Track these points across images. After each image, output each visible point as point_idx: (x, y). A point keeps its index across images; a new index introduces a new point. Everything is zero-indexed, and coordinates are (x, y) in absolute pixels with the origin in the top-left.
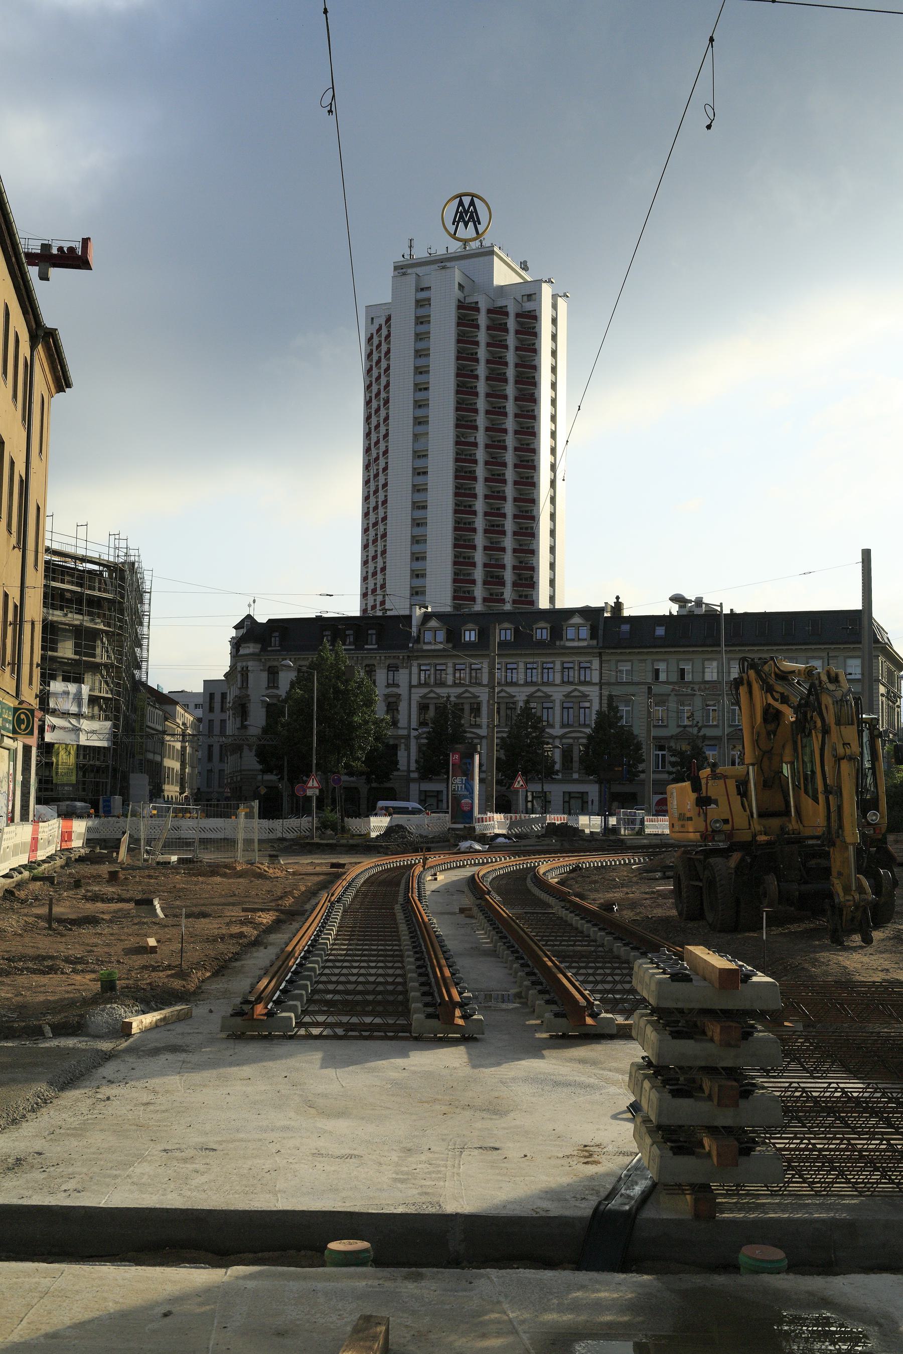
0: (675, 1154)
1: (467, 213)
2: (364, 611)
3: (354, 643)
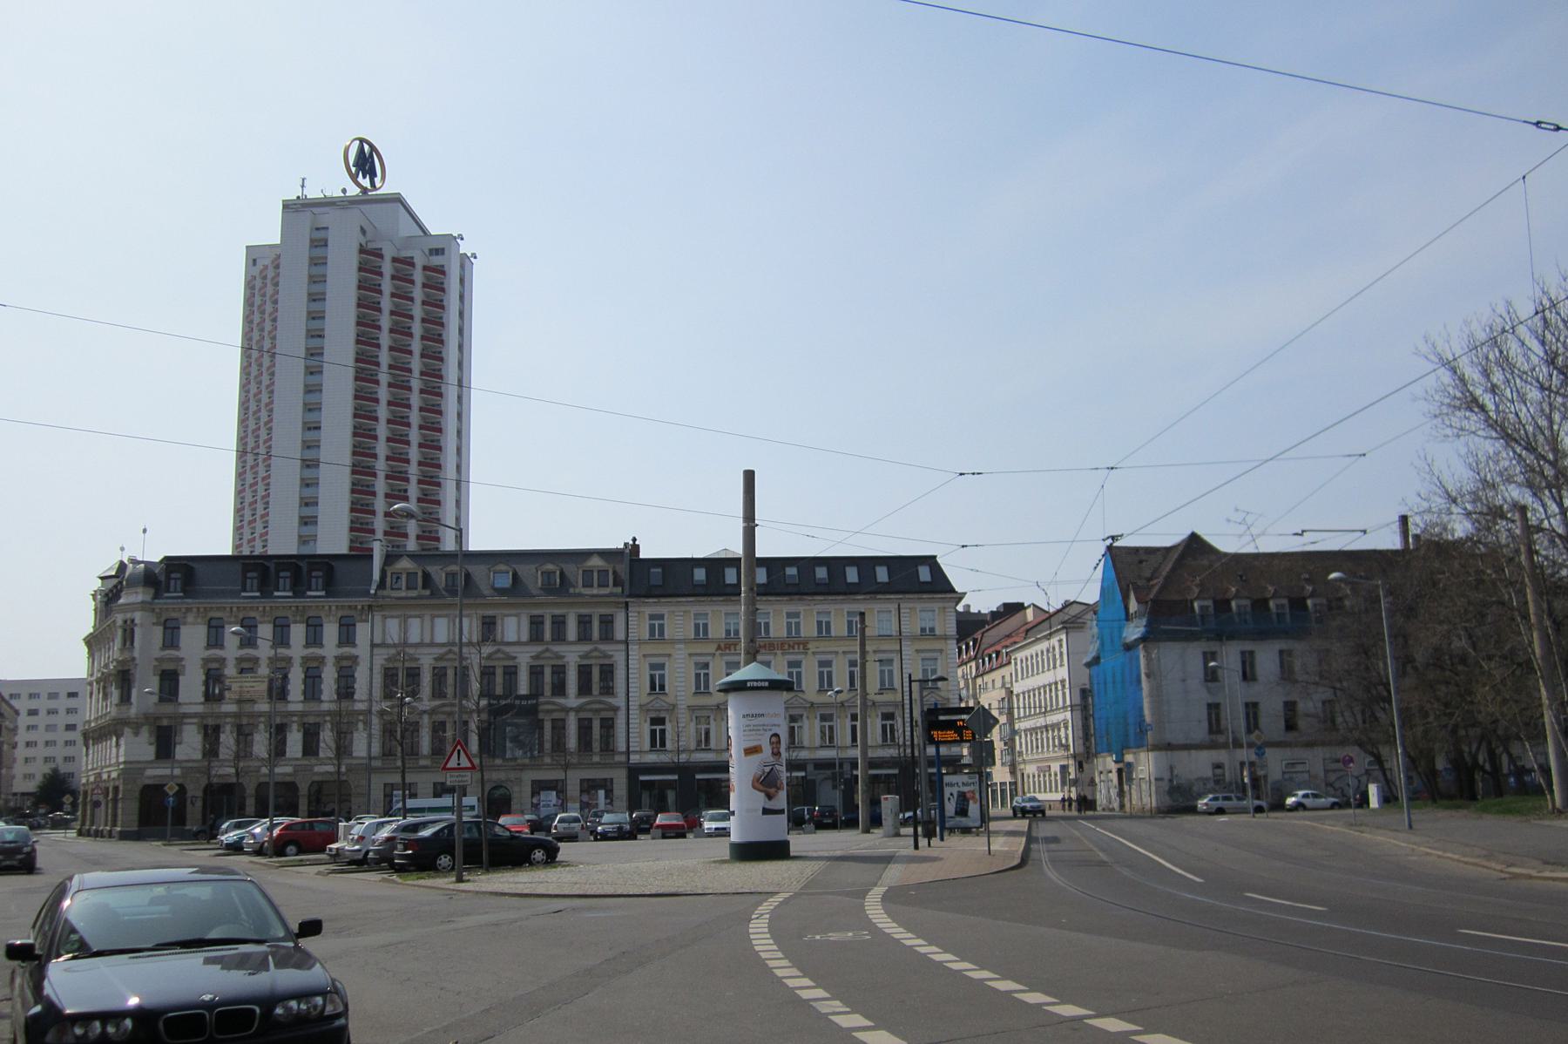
2: (236, 547)
3: (291, 589)
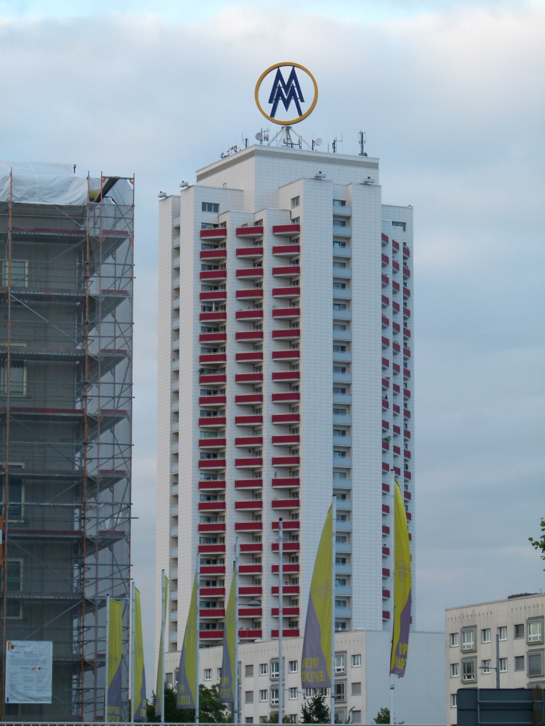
0: (403, 677)
1: (286, 91)
